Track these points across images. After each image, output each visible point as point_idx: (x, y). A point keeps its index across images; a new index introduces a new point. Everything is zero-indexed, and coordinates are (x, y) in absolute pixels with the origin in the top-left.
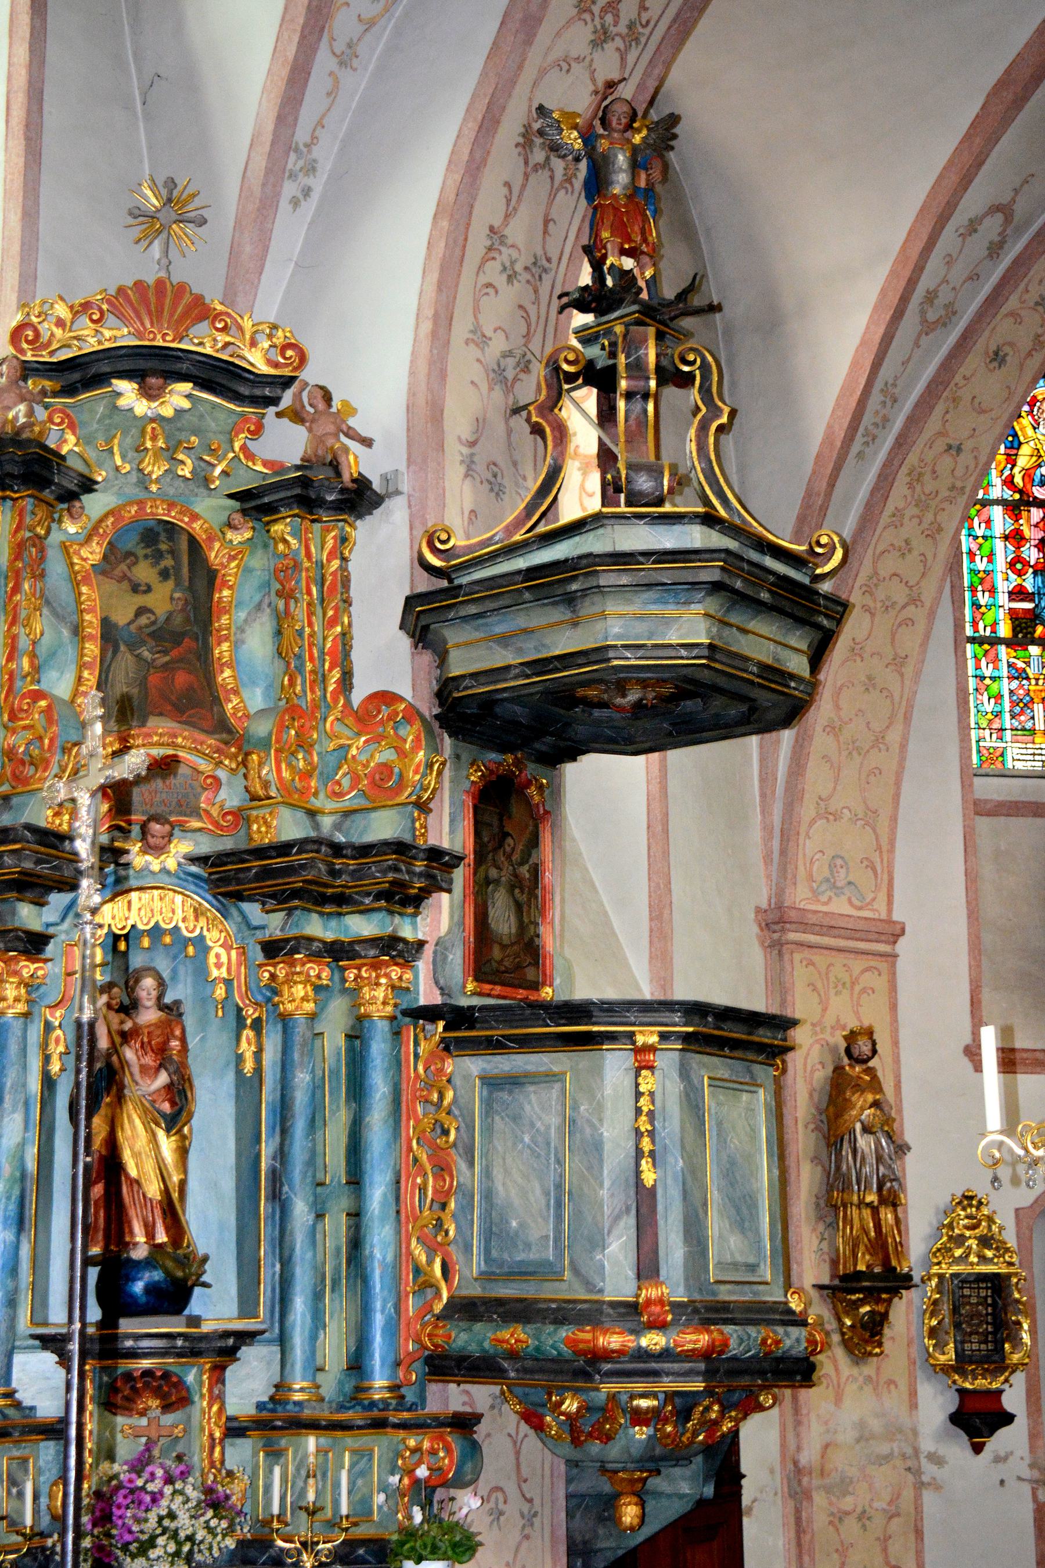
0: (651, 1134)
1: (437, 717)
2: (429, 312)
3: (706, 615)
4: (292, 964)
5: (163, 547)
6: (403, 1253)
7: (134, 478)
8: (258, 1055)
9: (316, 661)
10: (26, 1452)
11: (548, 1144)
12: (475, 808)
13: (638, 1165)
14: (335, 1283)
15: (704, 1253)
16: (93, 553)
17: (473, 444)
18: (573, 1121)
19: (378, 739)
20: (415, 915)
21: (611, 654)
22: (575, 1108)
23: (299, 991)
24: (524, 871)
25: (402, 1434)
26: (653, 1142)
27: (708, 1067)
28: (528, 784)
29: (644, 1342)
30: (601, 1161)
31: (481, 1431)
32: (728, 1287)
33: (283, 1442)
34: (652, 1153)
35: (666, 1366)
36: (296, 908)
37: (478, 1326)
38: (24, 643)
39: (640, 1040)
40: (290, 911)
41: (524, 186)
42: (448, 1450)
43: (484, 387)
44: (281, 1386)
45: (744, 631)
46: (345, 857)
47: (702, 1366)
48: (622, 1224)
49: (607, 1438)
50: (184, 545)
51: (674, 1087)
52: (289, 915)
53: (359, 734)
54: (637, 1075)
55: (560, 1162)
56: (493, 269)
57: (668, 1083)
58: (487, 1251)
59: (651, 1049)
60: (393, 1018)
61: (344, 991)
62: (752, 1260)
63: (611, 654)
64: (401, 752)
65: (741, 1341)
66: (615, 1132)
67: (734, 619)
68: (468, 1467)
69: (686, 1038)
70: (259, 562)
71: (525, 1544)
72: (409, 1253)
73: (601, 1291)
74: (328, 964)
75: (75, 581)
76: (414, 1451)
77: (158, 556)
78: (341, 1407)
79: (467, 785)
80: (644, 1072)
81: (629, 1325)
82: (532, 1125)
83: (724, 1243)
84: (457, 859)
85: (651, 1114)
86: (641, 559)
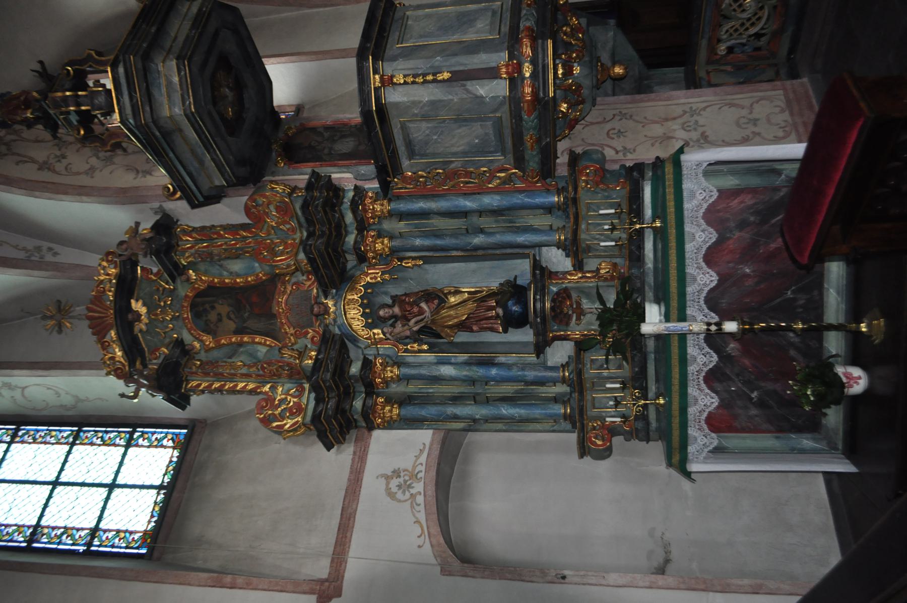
0: (424, 75)
1: (255, 185)
2: (78, 198)
3: (164, 62)
4: (367, 251)
5: (201, 309)
6: (496, 191)
7: (175, 322)
8: (414, 258)
9: (244, 239)
10: (589, 360)
11: (436, 127)
12: (296, 163)
13: (440, 81)
14: (511, 222)
15: (483, 42)
16: (208, 340)
17: (138, 172)
18: (423, 116)
19: (267, 214)
20: (344, 190)
21: (188, 112)
22: (416, 115)
23: (379, 246)
24: (326, 135)
25: (579, 189)
26: (429, 74)
27: (394, 46)
28: (287, 134)
29: (527, 75)
30: (440, 101)
31: (579, 150)
32: (502, 26)
33: (584, 245)
34: (434, 74)
35: (540, 61)
36: (342, 250)
37: (527, 157)
38: (244, 371)
39: (378, 84)
40: (344, 252)
41: (19, 155)
42: (587, 167)
43: (113, 167)
44: (559, 245)
45: (176, 38)
46: (314, 231)
47: (540, 41)
48: (470, 88)
49: (579, 87)
50: (199, 300)
51: (401, 64)
52: (346, 252)
53: (265, 222)
54: (396, 84)
55: (444, 120)
56: (60, 167)
57: (399, 67)
58: (491, 152)
59: (382, 78)
60: (390, 201)
61: (380, 223)
62: (490, 14)
63: (188, 112)
64: (269, 203)
65: (527, 19)
66: (425, 94)
67: (168, 44)
68: (595, 156)
69: (375, 60)
70: (202, 267)
71: (634, 117)
72: (496, 187)
73: (504, 97)
74: (368, 232)
75: (219, 346)
76: (587, 183)
77: (205, 310)
78: (568, 217)
79: (286, 167)
80: (395, 80)
81: (519, 82)
82: (428, 135)
83: (481, 30)
84: (314, 174)
85: (415, 76)
86: (135, 101)
